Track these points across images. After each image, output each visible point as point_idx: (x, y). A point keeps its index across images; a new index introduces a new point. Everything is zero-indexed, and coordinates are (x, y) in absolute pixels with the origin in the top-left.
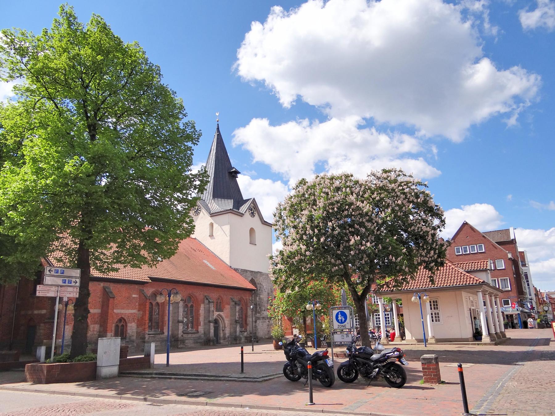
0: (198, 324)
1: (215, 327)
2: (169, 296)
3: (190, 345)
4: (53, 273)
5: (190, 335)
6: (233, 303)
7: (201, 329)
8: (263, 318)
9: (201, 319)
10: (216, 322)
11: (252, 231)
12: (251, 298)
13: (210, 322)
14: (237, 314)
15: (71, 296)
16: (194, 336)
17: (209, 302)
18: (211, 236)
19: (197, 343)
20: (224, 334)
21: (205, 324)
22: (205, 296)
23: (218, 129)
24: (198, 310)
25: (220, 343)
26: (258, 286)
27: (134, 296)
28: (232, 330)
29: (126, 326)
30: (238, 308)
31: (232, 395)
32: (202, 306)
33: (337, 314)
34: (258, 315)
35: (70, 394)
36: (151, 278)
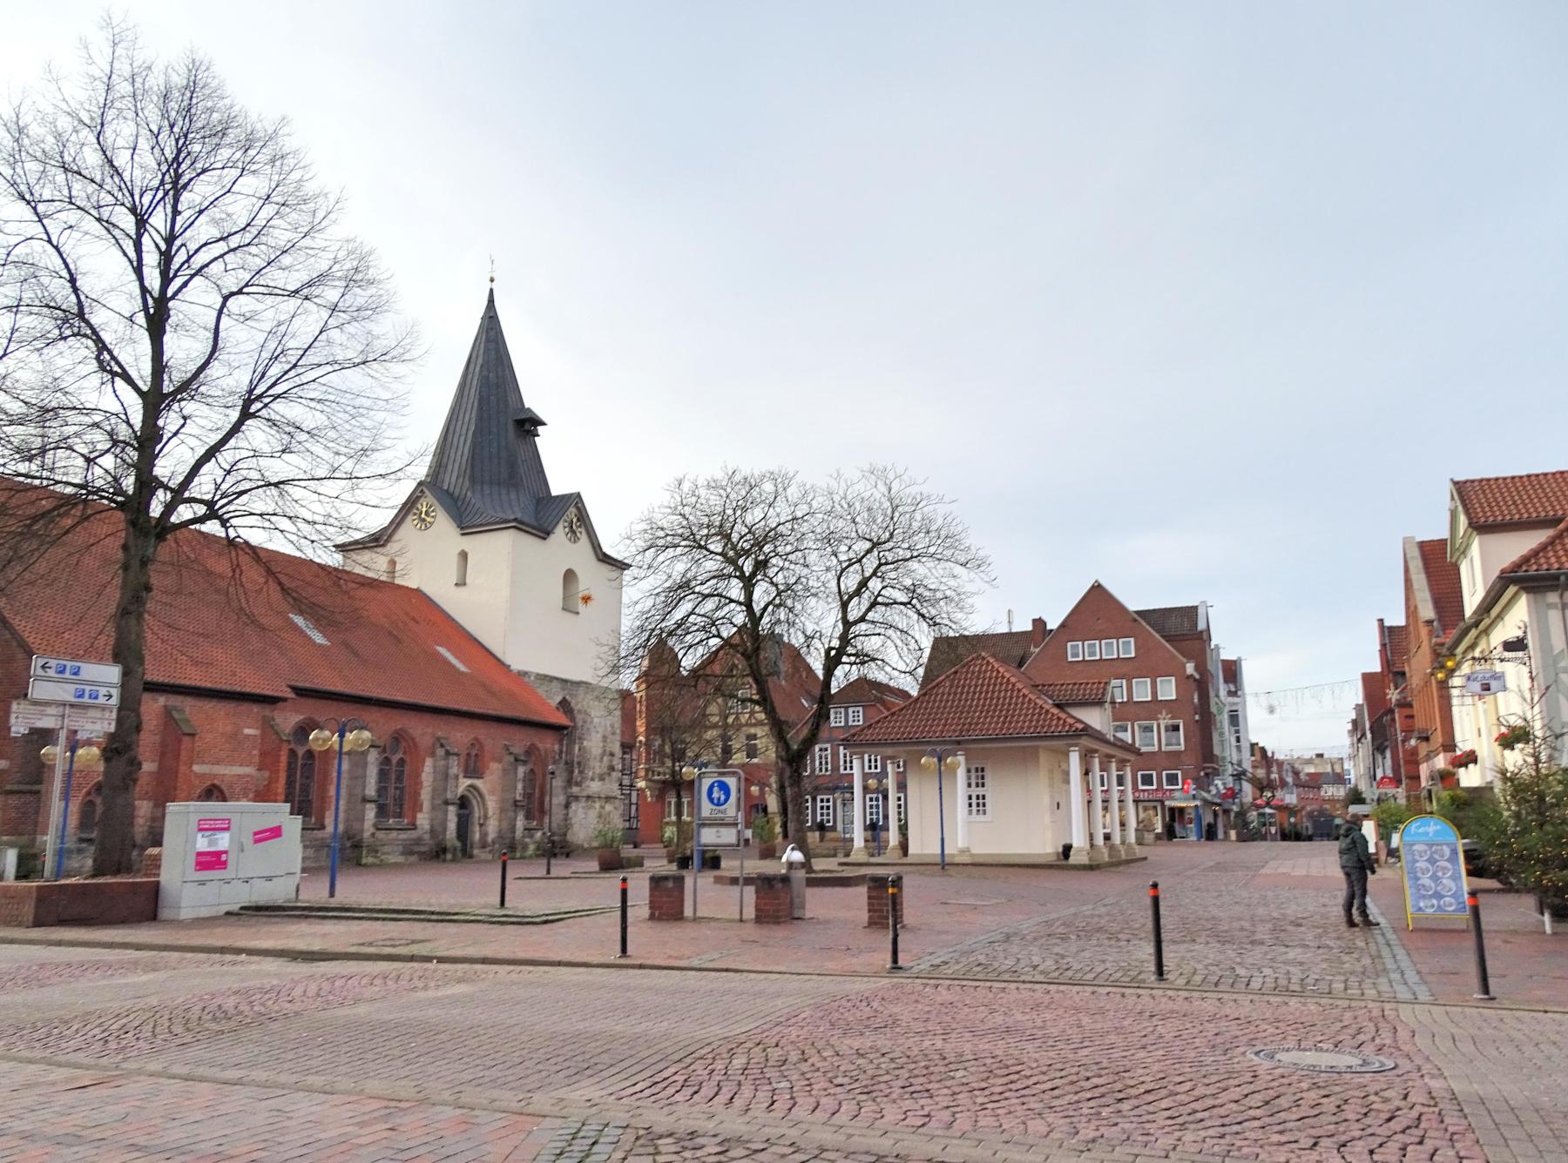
0: (417, 807)
1: (460, 816)
3: (392, 859)
5: (394, 834)
6: (512, 759)
7: (423, 820)
8: (588, 797)
9: (425, 795)
10: (463, 803)
11: (569, 576)
12: (557, 747)
13: (447, 803)
14: (520, 786)
16: (404, 836)
17: (448, 753)
18: (462, 583)
19: (412, 853)
20: (484, 835)
21: (434, 808)
22: (438, 739)
23: (491, 301)
24: (417, 774)
25: (471, 857)
26: (579, 717)
27: (247, 731)
28: (505, 825)
30: (521, 770)
32: (429, 762)
33: (712, 786)
34: (575, 790)
36: (294, 689)
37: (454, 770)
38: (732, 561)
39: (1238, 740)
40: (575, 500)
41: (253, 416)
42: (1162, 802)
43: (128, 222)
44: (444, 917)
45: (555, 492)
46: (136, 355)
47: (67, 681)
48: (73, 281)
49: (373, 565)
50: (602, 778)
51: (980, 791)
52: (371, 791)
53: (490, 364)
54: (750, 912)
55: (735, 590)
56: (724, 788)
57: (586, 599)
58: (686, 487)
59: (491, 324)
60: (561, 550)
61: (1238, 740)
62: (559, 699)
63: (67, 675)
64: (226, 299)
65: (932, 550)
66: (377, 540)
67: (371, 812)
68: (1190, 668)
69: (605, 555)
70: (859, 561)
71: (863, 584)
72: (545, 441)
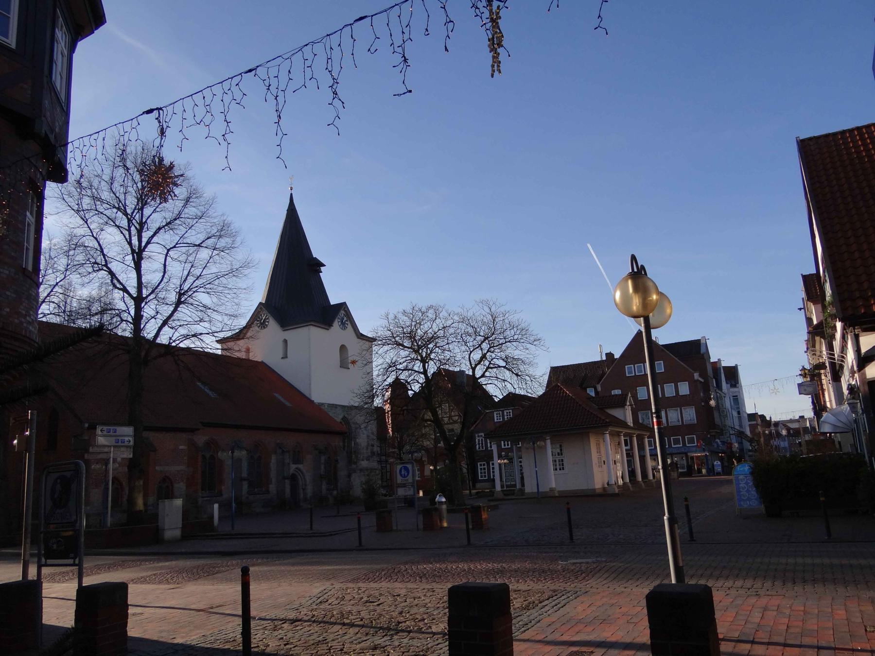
2: (233, 453)
4: (105, 433)
7: (273, 488)
9: (273, 474)
10: (293, 478)
11: (343, 348)
12: (341, 444)
14: (323, 467)
15: (125, 456)
18: (285, 357)
29: (172, 486)
31: (30, 218)
33: (401, 471)
34: (354, 466)
35: (850, 127)
37: (287, 461)
38: (416, 352)
39: (739, 413)
40: (343, 306)
41: (183, 303)
42: (686, 454)
43: (124, 223)
44: (285, 535)
45: (332, 303)
46: (129, 279)
47: (111, 436)
48: (102, 251)
49: (239, 351)
50: (368, 459)
51: (561, 457)
52: (245, 474)
53: (293, 236)
54: (421, 526)
55: (418, 366)
56: (407, 469)
57: (354, 362)
58: (391, 317)
59: (292, 212)
60: (336, 334)
61: (739, 413)
62: (341, 417)
63: (111, 433)
64: (168, 250)
65: (516, 337)
66: (239, 336)
67: (245, 486)
68: (696, 376)
69: (362, 335)
70: (480, 345)
71: (484, 357)
72: (325, 276)
